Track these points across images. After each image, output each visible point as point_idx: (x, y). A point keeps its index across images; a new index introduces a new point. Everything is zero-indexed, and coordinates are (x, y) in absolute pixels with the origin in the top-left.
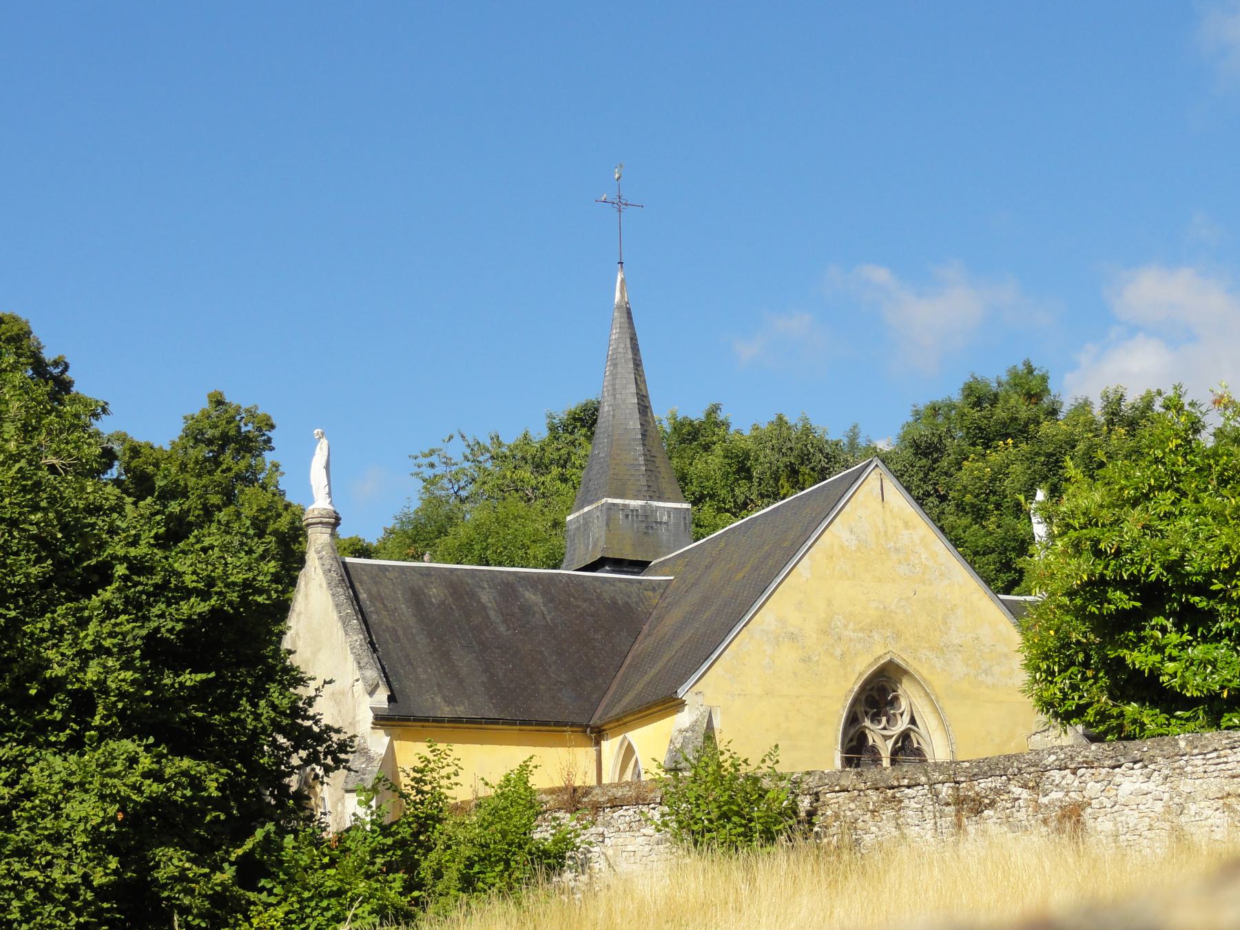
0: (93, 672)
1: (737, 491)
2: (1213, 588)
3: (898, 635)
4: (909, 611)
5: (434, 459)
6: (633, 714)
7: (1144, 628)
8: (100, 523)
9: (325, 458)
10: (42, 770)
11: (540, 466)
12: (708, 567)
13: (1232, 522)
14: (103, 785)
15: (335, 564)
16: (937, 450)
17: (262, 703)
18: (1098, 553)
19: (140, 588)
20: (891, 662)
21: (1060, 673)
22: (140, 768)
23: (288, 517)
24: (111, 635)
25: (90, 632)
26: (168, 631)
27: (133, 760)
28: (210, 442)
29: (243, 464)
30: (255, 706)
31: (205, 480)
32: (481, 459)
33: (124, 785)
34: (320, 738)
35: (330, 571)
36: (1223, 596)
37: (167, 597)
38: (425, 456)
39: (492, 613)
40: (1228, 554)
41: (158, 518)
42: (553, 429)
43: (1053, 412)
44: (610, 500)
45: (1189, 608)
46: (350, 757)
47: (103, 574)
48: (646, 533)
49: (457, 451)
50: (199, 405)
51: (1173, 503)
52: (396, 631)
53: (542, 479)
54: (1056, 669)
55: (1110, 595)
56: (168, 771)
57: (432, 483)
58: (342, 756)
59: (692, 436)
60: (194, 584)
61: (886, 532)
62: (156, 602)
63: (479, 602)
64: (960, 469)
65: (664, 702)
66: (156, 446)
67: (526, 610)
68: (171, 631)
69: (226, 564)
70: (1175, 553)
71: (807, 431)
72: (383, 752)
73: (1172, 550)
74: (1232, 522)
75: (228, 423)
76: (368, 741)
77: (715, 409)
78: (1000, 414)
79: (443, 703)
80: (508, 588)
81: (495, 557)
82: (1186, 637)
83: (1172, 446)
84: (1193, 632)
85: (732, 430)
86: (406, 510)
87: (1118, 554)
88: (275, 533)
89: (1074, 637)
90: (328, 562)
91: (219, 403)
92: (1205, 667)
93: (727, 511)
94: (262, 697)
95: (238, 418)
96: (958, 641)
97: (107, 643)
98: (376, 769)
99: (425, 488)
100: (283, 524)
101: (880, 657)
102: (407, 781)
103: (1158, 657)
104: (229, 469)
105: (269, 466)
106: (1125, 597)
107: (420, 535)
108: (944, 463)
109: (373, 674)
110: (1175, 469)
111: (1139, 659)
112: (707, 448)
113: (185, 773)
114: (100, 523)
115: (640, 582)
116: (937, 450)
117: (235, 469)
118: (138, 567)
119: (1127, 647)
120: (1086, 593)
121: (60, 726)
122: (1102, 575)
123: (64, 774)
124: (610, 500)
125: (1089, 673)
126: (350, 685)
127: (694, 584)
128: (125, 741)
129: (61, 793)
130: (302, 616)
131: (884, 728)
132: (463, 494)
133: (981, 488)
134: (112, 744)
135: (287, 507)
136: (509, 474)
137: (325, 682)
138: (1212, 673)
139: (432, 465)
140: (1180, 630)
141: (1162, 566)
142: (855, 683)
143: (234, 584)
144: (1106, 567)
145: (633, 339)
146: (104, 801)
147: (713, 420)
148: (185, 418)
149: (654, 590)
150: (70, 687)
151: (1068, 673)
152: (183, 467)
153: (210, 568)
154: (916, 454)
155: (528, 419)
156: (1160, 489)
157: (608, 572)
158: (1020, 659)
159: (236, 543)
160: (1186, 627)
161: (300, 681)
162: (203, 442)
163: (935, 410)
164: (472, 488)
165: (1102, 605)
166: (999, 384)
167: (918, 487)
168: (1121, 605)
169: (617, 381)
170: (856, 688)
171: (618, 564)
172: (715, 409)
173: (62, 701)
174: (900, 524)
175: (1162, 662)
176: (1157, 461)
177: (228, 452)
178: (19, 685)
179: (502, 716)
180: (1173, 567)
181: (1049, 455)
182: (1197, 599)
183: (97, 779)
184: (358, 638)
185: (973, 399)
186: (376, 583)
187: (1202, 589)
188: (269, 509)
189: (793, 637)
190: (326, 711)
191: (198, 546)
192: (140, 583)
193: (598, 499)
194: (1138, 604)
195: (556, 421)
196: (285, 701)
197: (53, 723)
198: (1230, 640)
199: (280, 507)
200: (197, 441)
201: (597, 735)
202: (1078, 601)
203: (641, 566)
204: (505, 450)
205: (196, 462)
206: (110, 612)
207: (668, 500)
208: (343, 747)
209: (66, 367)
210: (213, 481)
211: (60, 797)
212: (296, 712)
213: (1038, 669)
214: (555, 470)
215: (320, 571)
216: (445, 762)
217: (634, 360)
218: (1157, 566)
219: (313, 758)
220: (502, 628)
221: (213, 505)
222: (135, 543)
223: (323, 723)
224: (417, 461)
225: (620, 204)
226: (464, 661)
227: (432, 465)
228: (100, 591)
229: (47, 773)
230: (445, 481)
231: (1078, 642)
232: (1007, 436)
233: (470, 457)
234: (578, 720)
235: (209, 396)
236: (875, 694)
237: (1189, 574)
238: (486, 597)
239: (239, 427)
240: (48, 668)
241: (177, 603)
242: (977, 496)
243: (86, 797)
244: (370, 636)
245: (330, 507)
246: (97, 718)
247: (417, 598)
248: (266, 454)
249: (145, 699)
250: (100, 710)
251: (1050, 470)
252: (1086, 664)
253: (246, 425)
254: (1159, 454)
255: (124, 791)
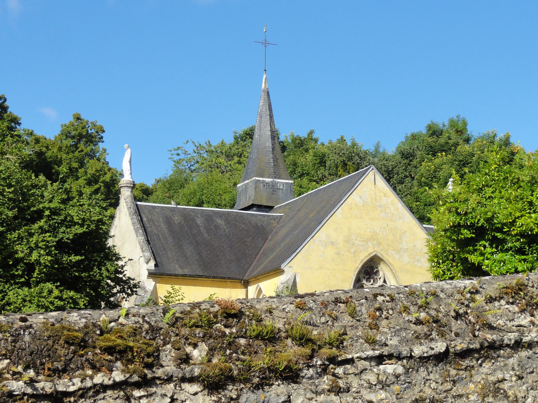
0: (34, 256)
1: (319, 173)
2: (504, 230)
3: (379, 244)
4: (384, 233)
5: (179, 152)
6: (262, 275)
7: (476, 245)
8: (37, 192)
9: (129, 157)
10: (14, 294)
11: (229, 157)
12: (299, 210)
13: (513, 202)
14: (39, 301)
15: (132, 205)
16: (412, 156)
17: (103, 268)
18: (458, 214)
19: (55, 221)
20: (376, 255)
21: (443, 263)
22: (53, 295)
23: (110, 175)
24: (43, 241)
25: (34, 239)
26: (67, 239)
27: (50, 292)
28: (73, 137)
29: (89, 149)
30: (100, 269)
31: (71, 155)
32: (202, 152)
33: (47, 301)
34: (125, 282)
35: (130, 208)
36: (508, 233)
37: (66, 225)
38: (175, 150)
39: (202, 229)
40: (511, 216)
41: (61, 190)
42: (236, 138)
43: (467, 141)
44: (257, 178)
45: (495, 237)
46: (138, 289)
47: (39, 215)
48: (273, 194)
49: (190, 148)
50: (69, 119)
51: (492, 192)
52: (159, 236)
53: (229, 163)
54: (441, 261)
55: (462, 231)
56: (64, 296)
57: (178, 163)
58: (135, 289)
59: (300, 144)
60: (78, 221)
61: (376, 198)
62: (61, 226)
63: (196, 223)
64: (421, 165)
65: (275, 270)
66: (48, 138)
67: (217, 227)
68: (67, 239)
69: (90, 212)
70: (490, 214)
71: (354, 145)
72: (152, 289)
73: (488, 213)
74: (513, 202)
75: (83, 128)
76: (146, 284)
77: (312, 132)
78: (442, 140)
79: (179, 268)
80: (209, 217)
81: (206, 199)
82: (494, 250)
83: (493, 167)
84: (497, 248)
85: (319, 143)
86: (165, 175)
87: (466, 213)
88: (103, 182)
89: (448, 248)
90: (129, 204)
91: (78, 119)
92: (500, 264)
93: (315, 181)
94: (104, 266)
95: (87, 126)
96: (406, 247)
97: (40, 245)
98: (149, 296)
99: (175, 165)
100: (107, 178)
101: (371, 253)
102: (162, 302)
103: (482, 258)
104: (82, 151)
105: (101, 150)
106: (469, 232)
107: (172, 187)
108: (415, 162)
109: (148, 254)
110: (493, 178)
111: (474, 258)
112: (307, 151)
113: (71, 298)
114: (37, 192)
115: (269, 216)
116: (412, 156)
117: (85, 151)
118: (55, 212)
119: (469, 253)
120: (452, 230)
121: (21, 276)
122: (459, 223)
123: (23, 296)
124: (257, 178)
125: (454, 264)
126: (138, 259)
127: (292, 218)
128: (47, 283)
129: (22, 303)
130: (117, 228)
131: (372, 284)
132: (193, 168)
133: (429, 175)
134: (42, 284)
135: (109, 169)
136: (214, 160)
137: (129, 260)
138: (503, 266)
139: (178, 155)
140: (492, 247)
141: (484, 220)
142: (359, 264)
143: (94, 220)
144: (461, 219)
145: (270, 105)
146: (39, 308)
147: (311, 138)
148: (62, 125)
149: (274, 220)
150: (25, 261)
151: (446, 264)
152: (60, 149)
153: (84, 213)
154: (402, 158)
155: (224, 136)
156: (487, 186)
157: (255, 211)
158: (427, 257)
159: (94, 203)
160: (494, 246)
161: (118, 259)
162: (70, 137)
163: (414, 137)
164: (197, 165)
165: (458, 235)
166: (444, 126)
167: (402, 173)
168: (466, 236)
169: (262, 124)
170: (360, 266)
171: (260, 207)
172: (312, 132)
173: (22, 267)
174: (382, 195)
175: (483, 260)
176: (486, 174)
177: (82, 143)
178: (5, 259)
179: (204, 274)
180: (489, 220)
181: (460, 161)
182: (498, 234)
183: (36, 298)
184: (142, 238)
185: (431, 132)
186: (150, 214)
187: (500, 230)
188: (101, 170)
189: (333, 243)
190: (129, 272)
191: (78, 204)
192: (55, 219)
193: (252, 178)
194: (473, 236)
195: (238, 135)
196: (113, 268)
197: (18, 275)
198: (513, 251)
199: (106, 170)
200: (67, 136)
201: (246, 284)
202: (448, 234)
203: (270, 208)
204: (212, 148)
205: (67, 147)
206: (42, 230)
207: (283, 179)
208: (135, 286)
209: (5, 100)
210: (74, 156)
211: (21, 305)
212: (117, 272)
213: (434, 261)
214: (236, 159)
215: (126, 208)
216: (178, 294)
217: (270, 115)
218: (482, 219)
219: (122, 291)
220: (206, 235)
221: (74, 168)
222: (51, 201)
223: (127, 276)
224: (171, 152)
225: (265, 43)
226: (189, 250)
227: (178, 155)
228: (38, 222)
229: (16, 295)
230: (185, 162)
231: (450, 251)
232: (443, 151)
233: (196, 151)
234: (238, 277)
235: (73, 115)
236: (368, 269)
237: (495, 224)
238: (199, 221)
239: (88, 131)
240: (17, 253)
241: (70, 228)
242: (427, 178)
243: (32, 306)
244: (147, 238)
245: (131, 180)
246: (35, 274)
247: (169, 222)
248: (100, 144)
249: (55, 268)
250: (37, 271)
251: (461, 168)
252: (453, 260)
253: (91, 130)
254: (487, 171)
255: (47, 304)
